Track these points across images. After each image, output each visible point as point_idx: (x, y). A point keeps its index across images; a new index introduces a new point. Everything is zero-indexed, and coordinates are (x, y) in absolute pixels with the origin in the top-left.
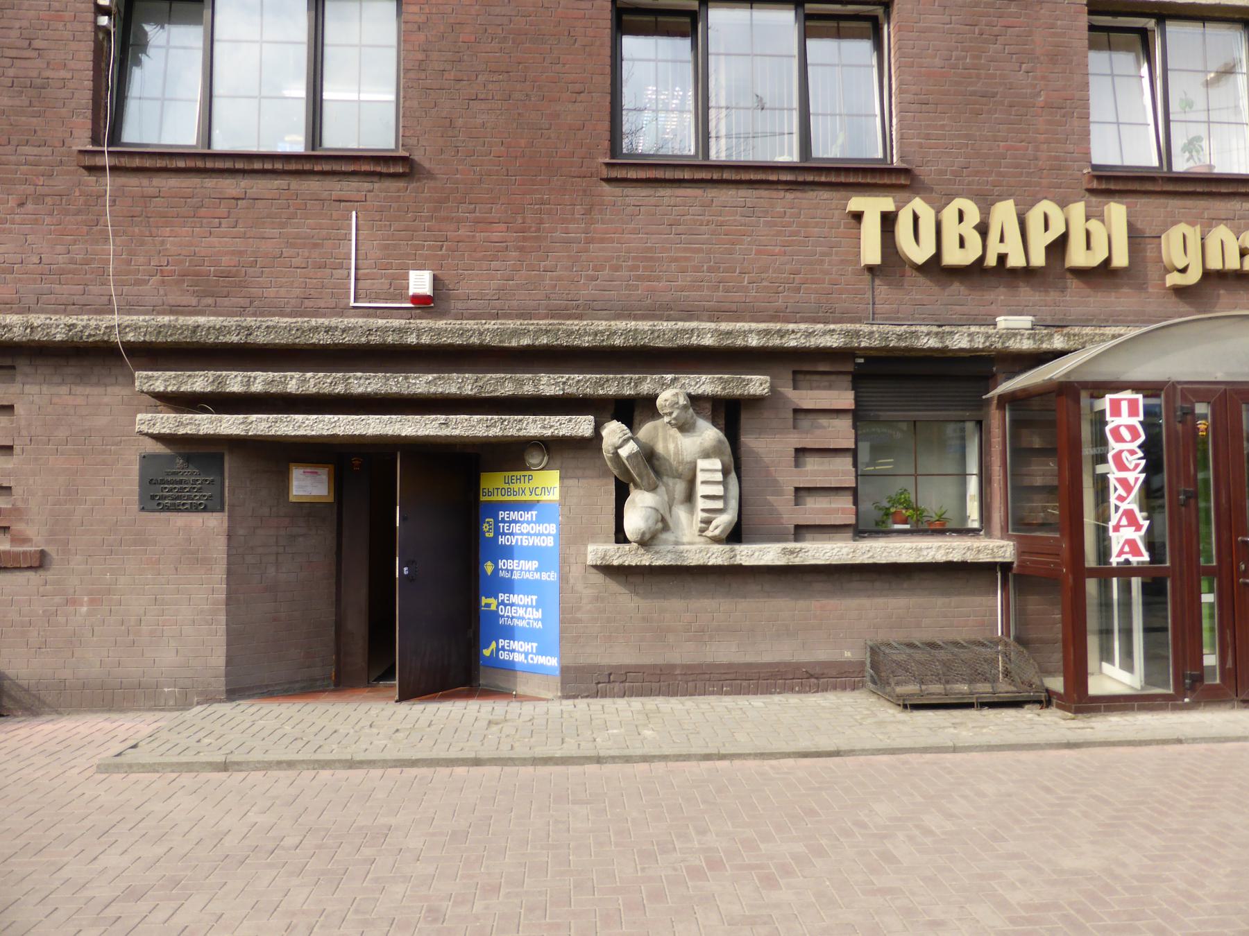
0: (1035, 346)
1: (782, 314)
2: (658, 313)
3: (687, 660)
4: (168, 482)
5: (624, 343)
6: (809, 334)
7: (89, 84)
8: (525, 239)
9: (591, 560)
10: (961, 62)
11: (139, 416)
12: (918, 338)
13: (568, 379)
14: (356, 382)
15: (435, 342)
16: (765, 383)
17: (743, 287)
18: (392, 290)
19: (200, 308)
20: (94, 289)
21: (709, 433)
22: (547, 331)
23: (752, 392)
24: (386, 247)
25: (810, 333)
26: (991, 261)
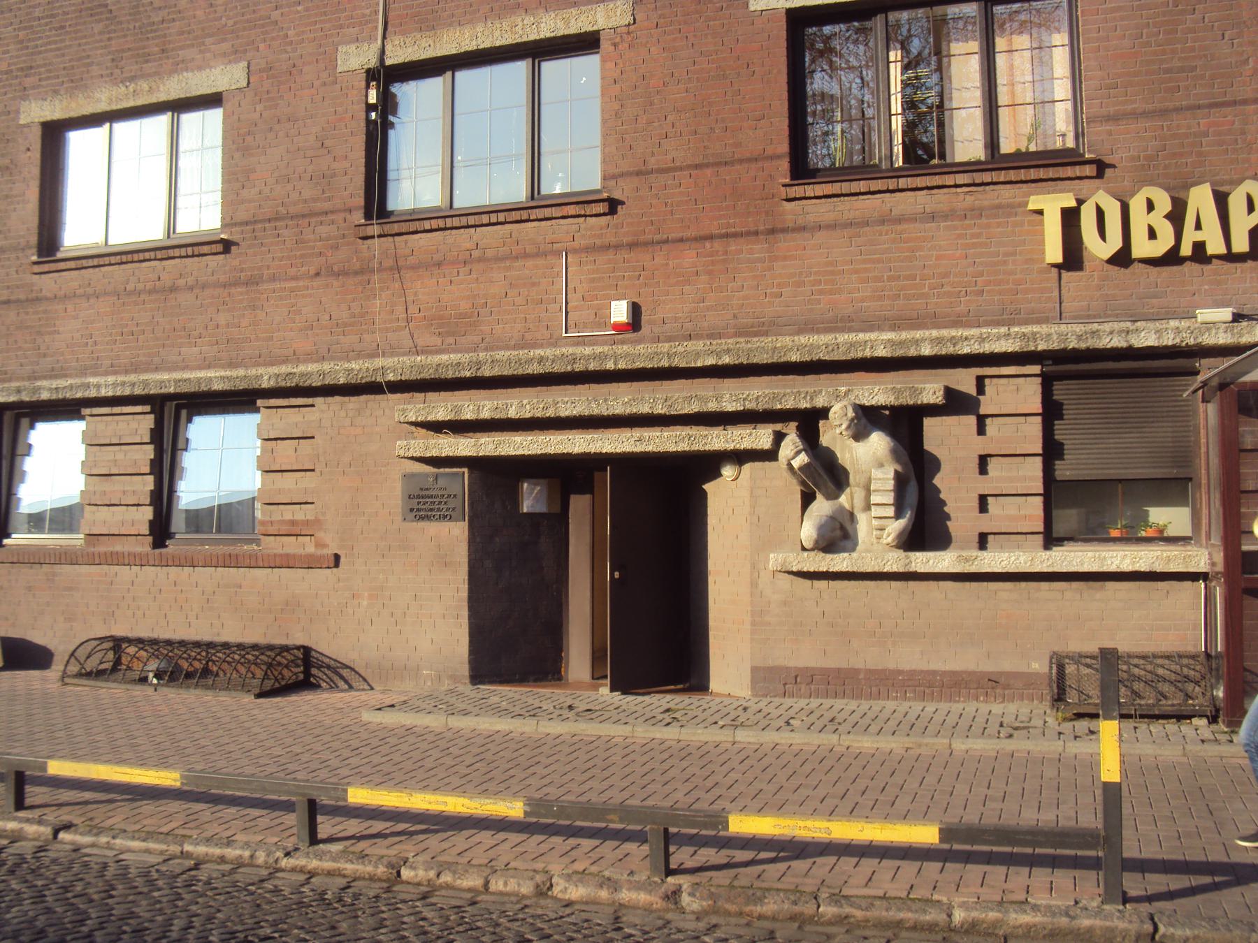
0: (1232, 341)
1: (964, 319)
2: (840, 325)
3: (871, 665)
4: (423, 497)
6: (982, 340)
7: (362, 169)
8: (713, 263)
9: (772, 565)
10: (1153, 39)
11: (398, 443)
12: (1100, 338)
15: (630, 367)
20: (367, 337)
21: (878, 442)
22: (729, 350)
23: (925, 401)
24: (592, 280)
26: (1186, 250)
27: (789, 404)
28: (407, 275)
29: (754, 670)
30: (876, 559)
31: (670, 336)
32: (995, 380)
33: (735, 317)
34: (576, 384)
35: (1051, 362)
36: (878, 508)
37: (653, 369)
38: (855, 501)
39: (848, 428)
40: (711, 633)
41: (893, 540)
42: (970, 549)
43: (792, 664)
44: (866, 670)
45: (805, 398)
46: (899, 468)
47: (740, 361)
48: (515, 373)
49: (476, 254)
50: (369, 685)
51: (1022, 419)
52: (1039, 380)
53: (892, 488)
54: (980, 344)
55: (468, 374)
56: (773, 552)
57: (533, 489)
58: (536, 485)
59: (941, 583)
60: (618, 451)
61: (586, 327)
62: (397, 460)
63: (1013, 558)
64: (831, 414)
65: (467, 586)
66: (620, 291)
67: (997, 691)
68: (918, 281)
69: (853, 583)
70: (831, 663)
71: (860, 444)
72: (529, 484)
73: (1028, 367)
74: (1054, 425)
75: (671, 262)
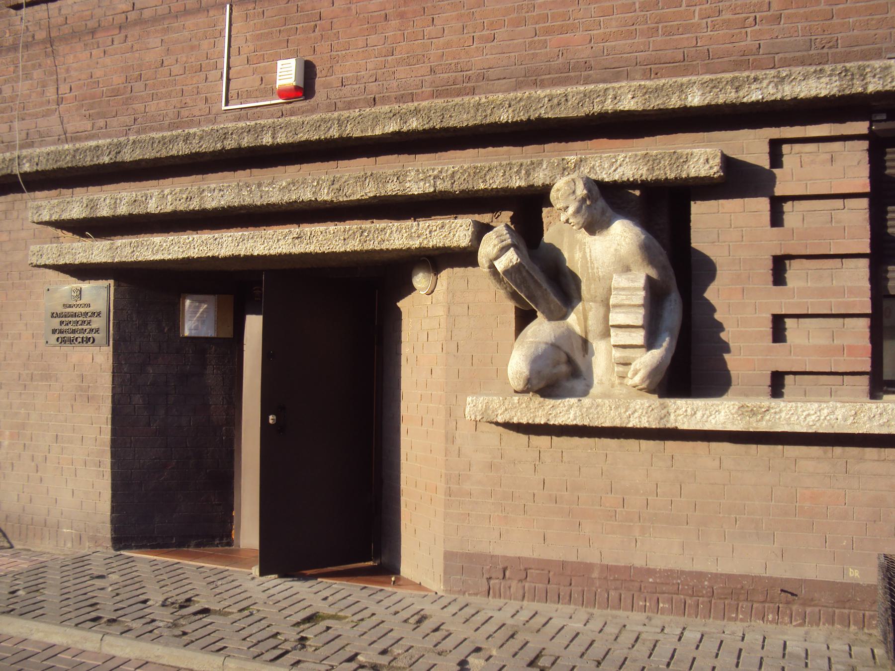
1: (751, 58)
2: (572, 74)
5: (513, 118)
13: (441, 172)
14: (209, 195)
15: (291, 140)
16: (714, 158)
17: (693, 25)
18: (263, 86)
19: (94, 131)
22: (417, 111)
23: (693, 174)
25: (784, 78)
27: (496, 182)
28: (62, 48)
29: (449, 556)
30: (617, 408)
31: (349, 102)
32: (797, 147)
33: (432, 71)
34: (235, 170)
35: (884, 117)
36: (620, 332)
37: (319, 141)
38: (590, 322)
39: (578, 211)
40: (403, 499)
41: (643, 381)
42: (758, 395)
43: (499, 550)
44: (602, 566)
45: (518, 172)
46: (654, 274)
47: (431, 125)
48: (158, 155)
49: (132, 16)
50: (9, 542)
51: (838, 203)
52: (865, 144)
53: (640, 301)
54: (776, 85)
55: (106, 160)
56: (474, 393)
57: (199, 308)
58: (201, 302)
59: (714, 445)
60: (272, 252)
61: (250, 95)
62: (30, 267)
63: (826, 412)
64: (553, 195)
65: (110, 426)
66: (292, 47)
67: (795, 607)
68: (683, 8)
69: (585, 441)
70: (555, 553)
71: (596, 237)
72: (193, 300)
73: (848, 124)
74: (886, 213)
75: (353, 6)
